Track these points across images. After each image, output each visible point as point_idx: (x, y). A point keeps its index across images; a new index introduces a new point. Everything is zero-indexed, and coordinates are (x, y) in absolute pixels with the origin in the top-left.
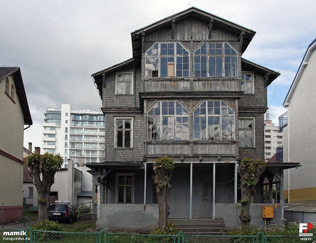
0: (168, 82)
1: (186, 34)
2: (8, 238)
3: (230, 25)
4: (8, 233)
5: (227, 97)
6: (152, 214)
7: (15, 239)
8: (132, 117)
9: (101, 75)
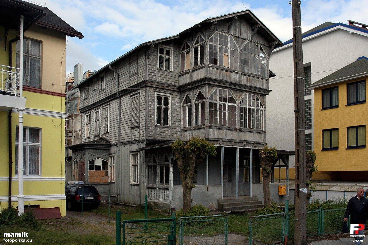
0: (224, 72)
1: (237, 29)
2: (8, 240)
3: (270, 33)
4: (9, 234)
5: (261, 93)
6: (213, 194)
7: (16, 241)
8: (170, 94)
9: (151, 45)
